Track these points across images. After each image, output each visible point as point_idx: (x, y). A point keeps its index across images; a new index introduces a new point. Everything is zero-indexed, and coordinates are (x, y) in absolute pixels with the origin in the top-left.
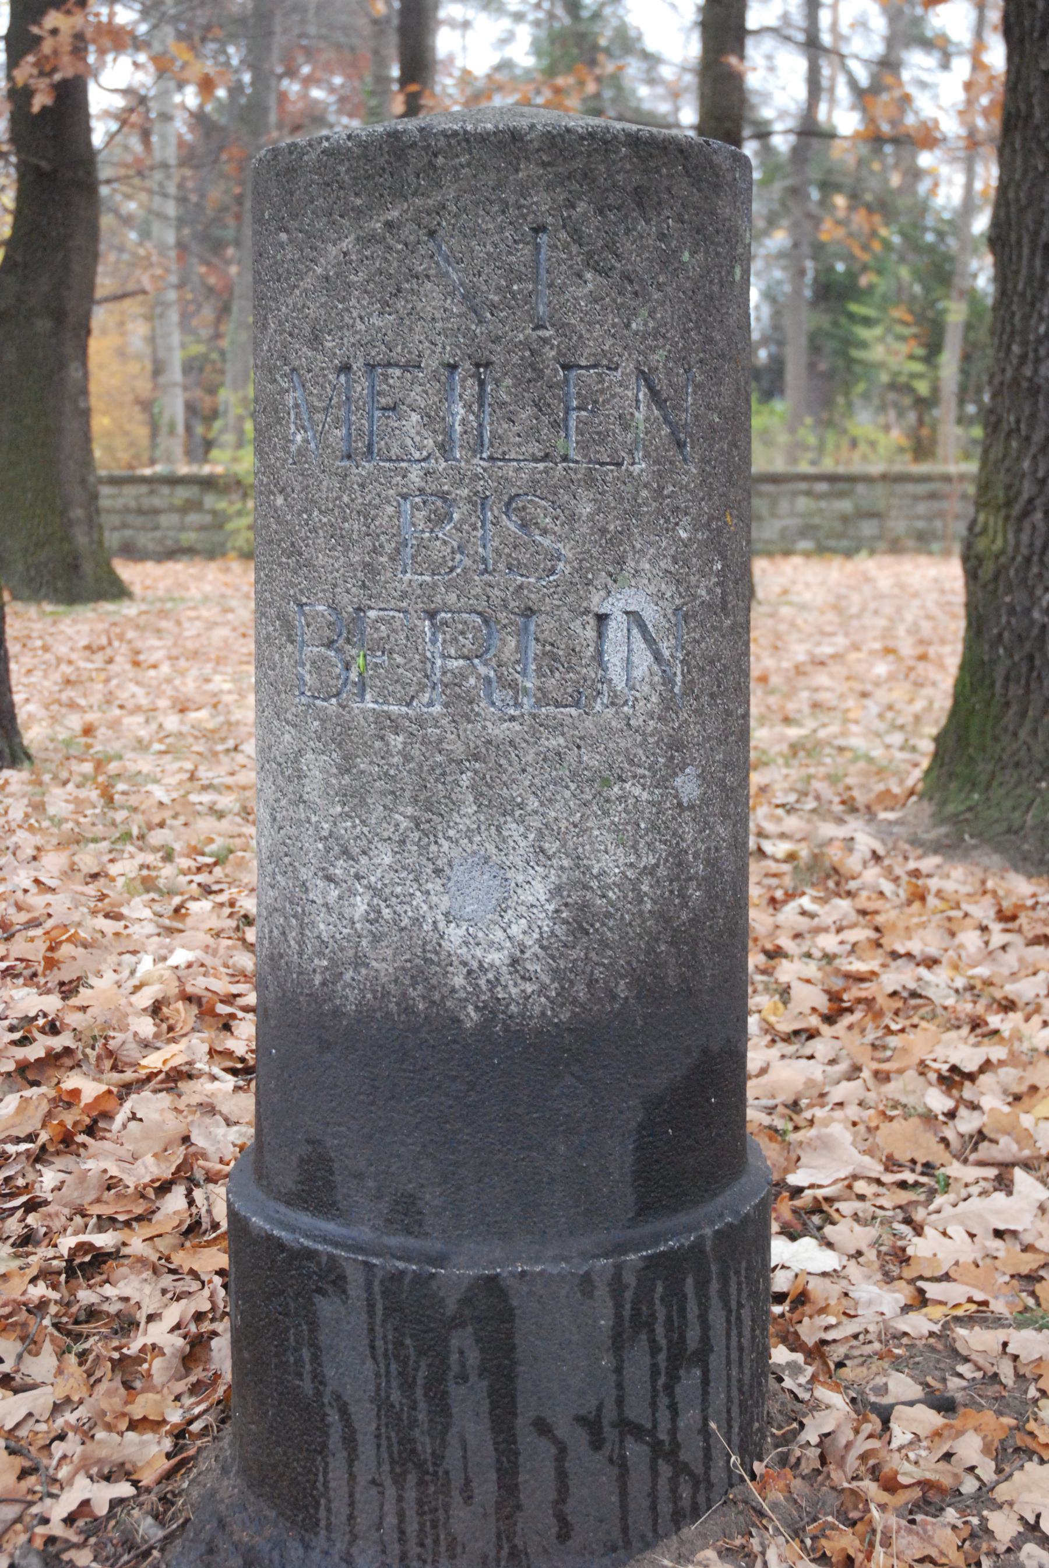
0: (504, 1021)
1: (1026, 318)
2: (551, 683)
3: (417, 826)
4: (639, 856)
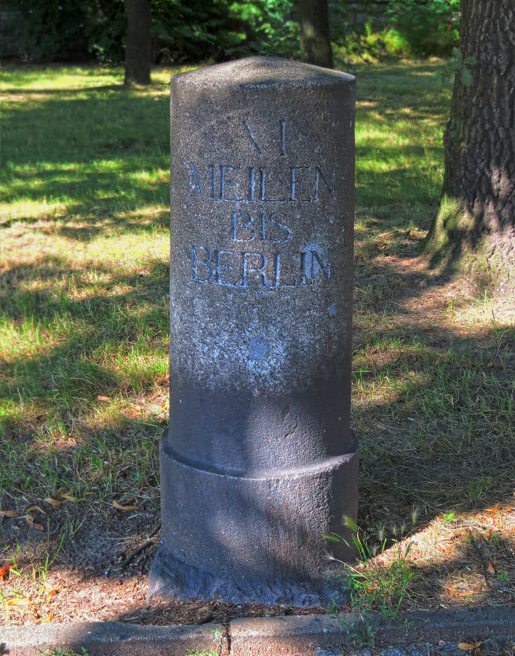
0: (267, 394)
1: (475, 31)
2: (285, 277)
3: (237, 326)
4: (315, 336)
